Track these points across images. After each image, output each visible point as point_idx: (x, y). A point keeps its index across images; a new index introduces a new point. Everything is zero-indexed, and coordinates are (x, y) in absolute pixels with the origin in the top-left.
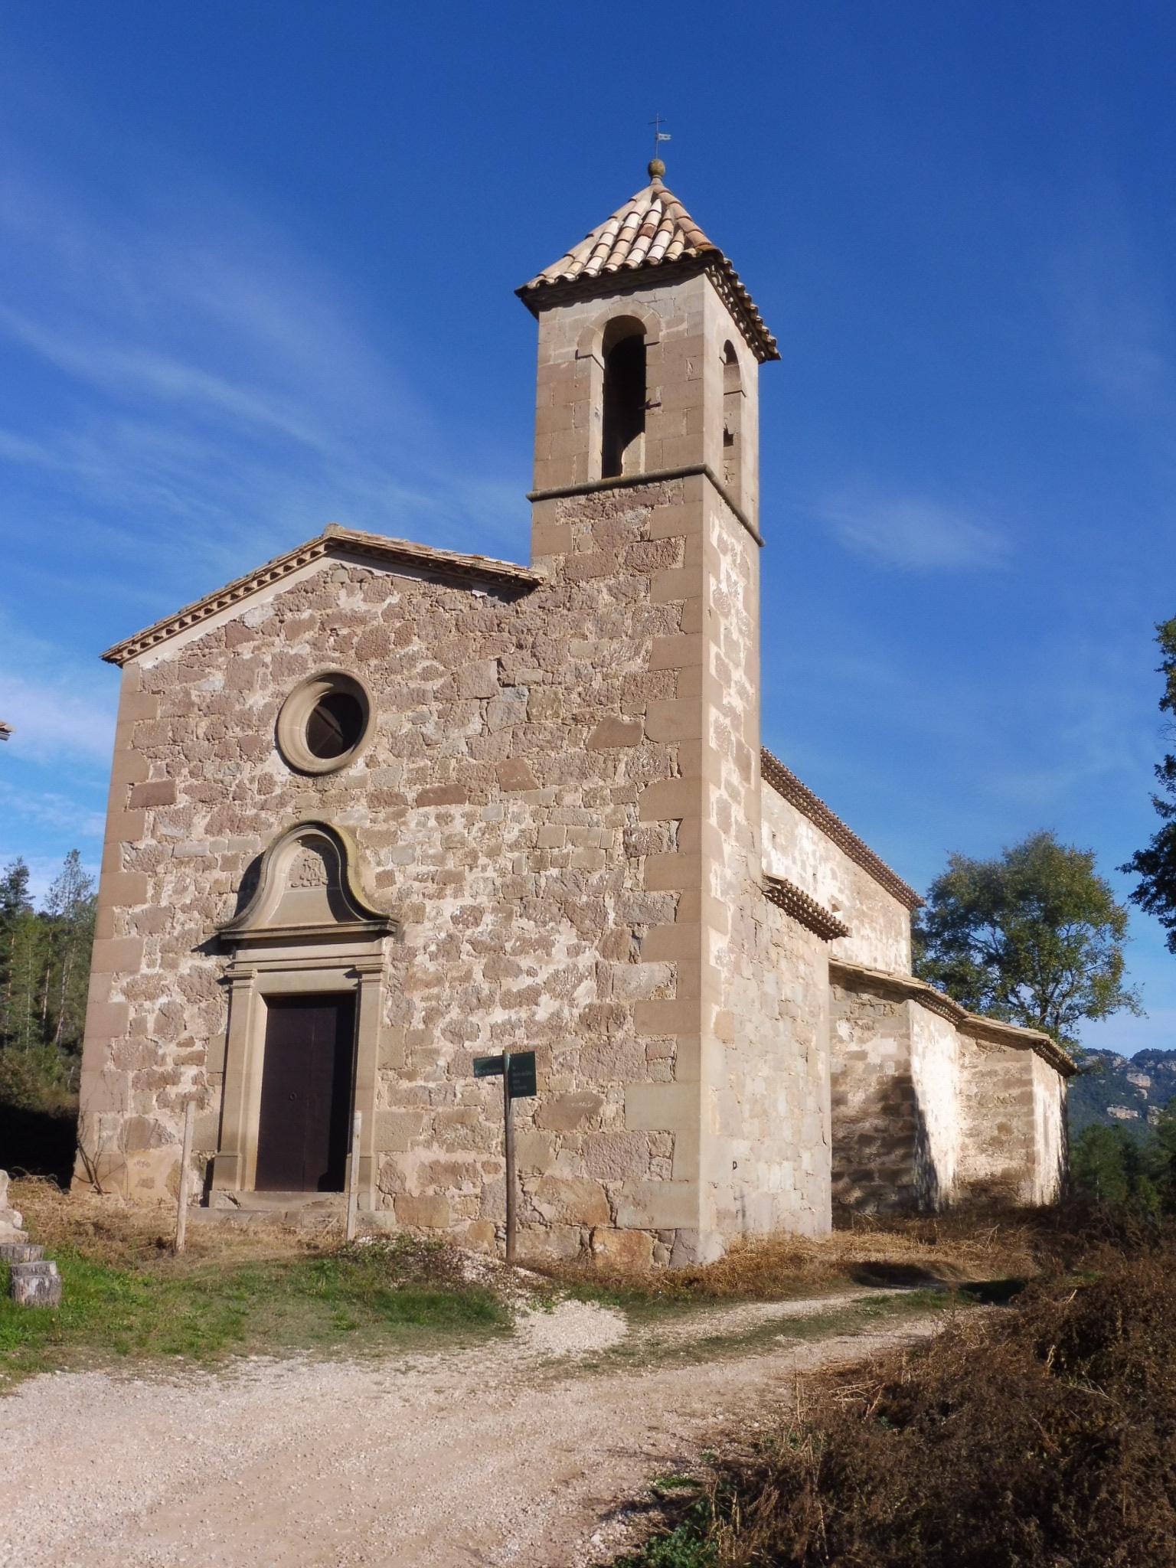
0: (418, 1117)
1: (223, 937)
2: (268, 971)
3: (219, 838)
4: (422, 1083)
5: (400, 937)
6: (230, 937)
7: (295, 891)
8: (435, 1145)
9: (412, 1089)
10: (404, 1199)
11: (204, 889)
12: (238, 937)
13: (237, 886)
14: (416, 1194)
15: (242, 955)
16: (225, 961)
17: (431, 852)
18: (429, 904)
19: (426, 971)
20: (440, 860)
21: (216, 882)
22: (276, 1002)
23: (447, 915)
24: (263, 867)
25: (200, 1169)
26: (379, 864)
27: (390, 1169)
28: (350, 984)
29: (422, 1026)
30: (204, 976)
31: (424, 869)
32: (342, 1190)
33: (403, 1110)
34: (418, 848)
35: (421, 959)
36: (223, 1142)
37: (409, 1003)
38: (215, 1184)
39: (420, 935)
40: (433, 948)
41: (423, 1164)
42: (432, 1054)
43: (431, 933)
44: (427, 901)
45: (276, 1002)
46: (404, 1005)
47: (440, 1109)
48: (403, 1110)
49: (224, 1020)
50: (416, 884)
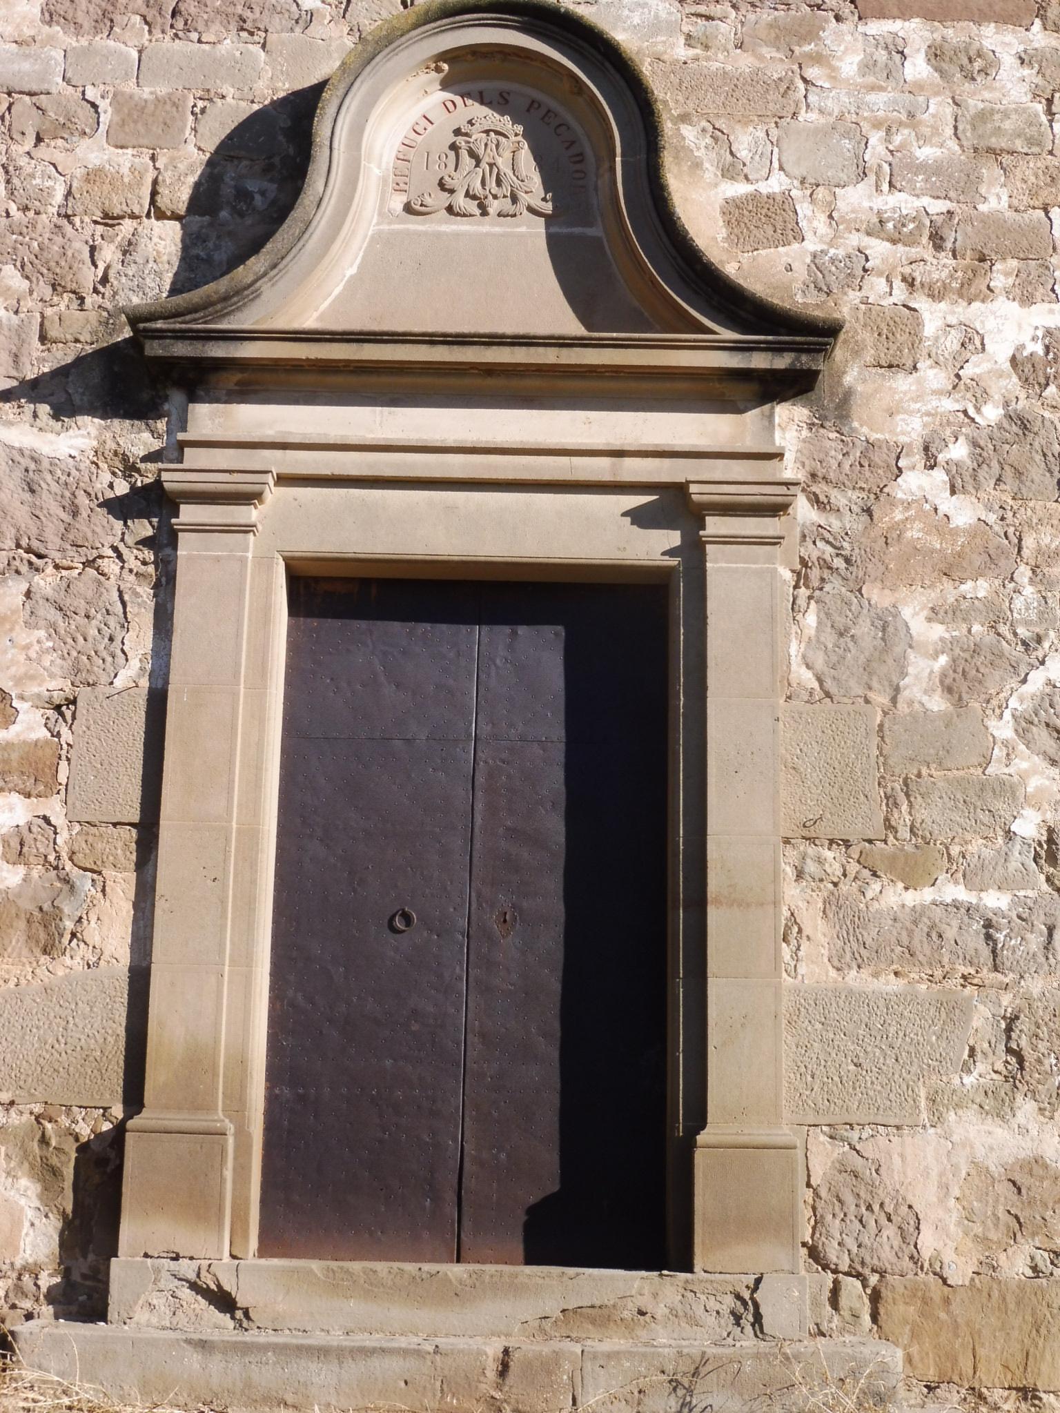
0: (955, 1012)
1: (154, 349)
2: (309, 483)
3: (101, 41)
4: (955, 892)
5: (837, 413)
6: (182, 349)
7: (415, 225)
8: (1026, 1109)
9: (917, 914)
10: (919, 1295)
11: (44, 194)
12: (218, 351)
13: (179, 195)
14: (960, 1271)
15: (207, 418)
16: (139, 439)
17: (926, 153)
18: (934, 317)
19: (941, 524)
20: (966, 186)
21: (94, 175)
22: (327, 594)
23: (1000, 351)
24: (322, 129)
25: (47, 1173)
26: (731, 171)
27: (861, 1190)
28: (654, 547)
29: (938, 703)
30: (48, 484)
31: (903, 203)
32: (685, 1264)
33: (893, 985)
34: (876, 138)
35: (917, 482)
36: (155, 1078)
37: (886, 624)
38: (133, 1231)
39: (899, 405)
40: (959, 451)
41: (979, 1168)
42: (991, 798)
43: (948, 405)
44: (921, 303)
45: (327, 594)
46: (864, 629)
47: (1035, 985)
48: (893, 985)
49: (140, 640)
50: (878, 249)
